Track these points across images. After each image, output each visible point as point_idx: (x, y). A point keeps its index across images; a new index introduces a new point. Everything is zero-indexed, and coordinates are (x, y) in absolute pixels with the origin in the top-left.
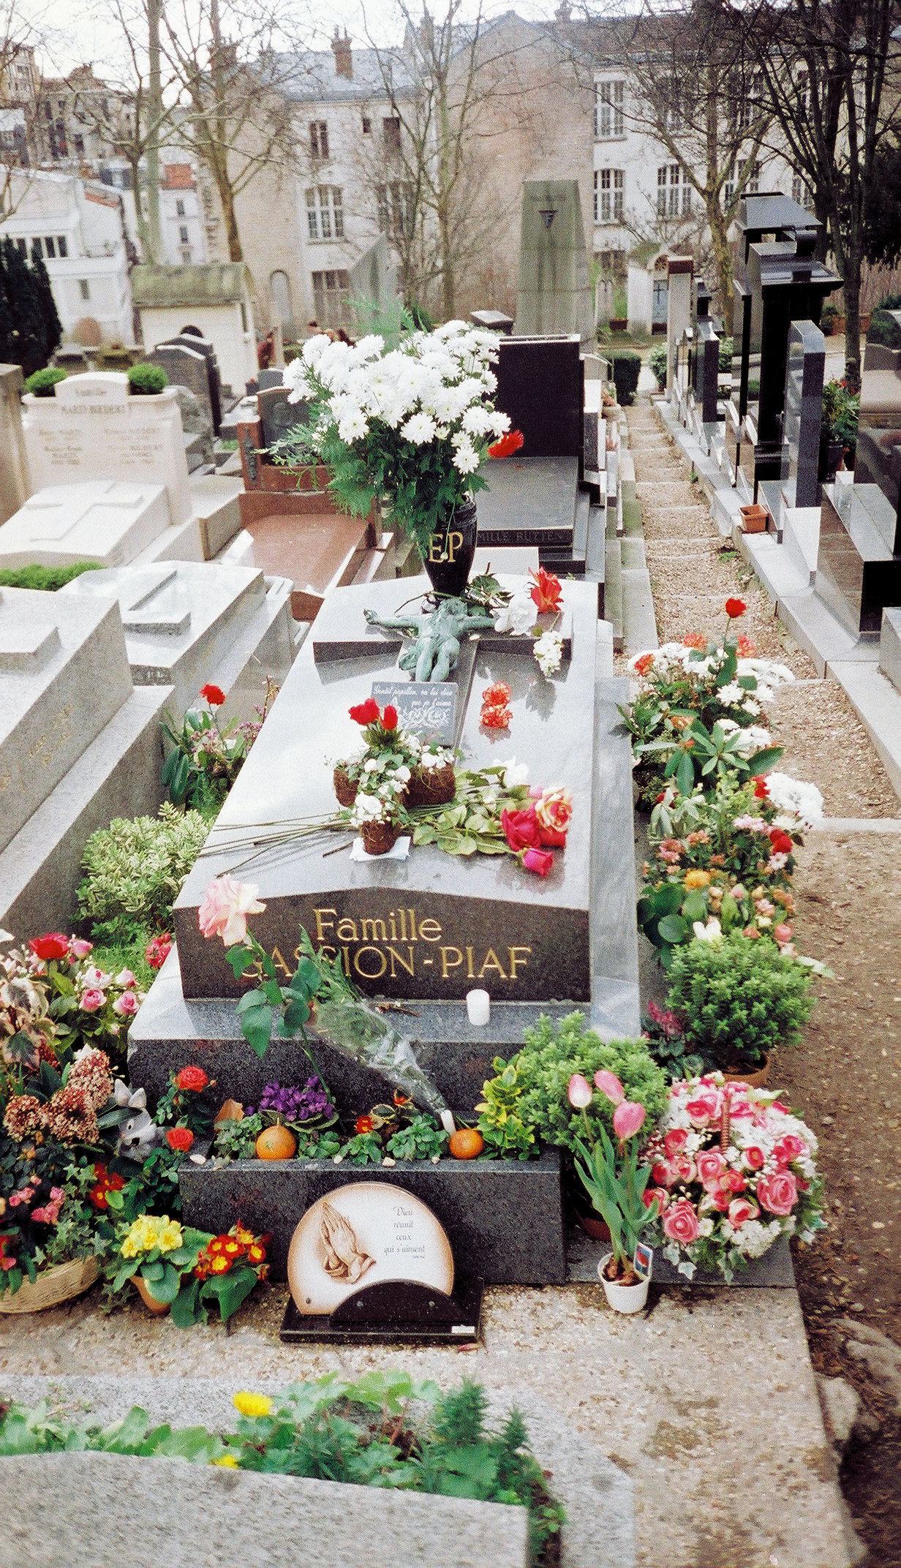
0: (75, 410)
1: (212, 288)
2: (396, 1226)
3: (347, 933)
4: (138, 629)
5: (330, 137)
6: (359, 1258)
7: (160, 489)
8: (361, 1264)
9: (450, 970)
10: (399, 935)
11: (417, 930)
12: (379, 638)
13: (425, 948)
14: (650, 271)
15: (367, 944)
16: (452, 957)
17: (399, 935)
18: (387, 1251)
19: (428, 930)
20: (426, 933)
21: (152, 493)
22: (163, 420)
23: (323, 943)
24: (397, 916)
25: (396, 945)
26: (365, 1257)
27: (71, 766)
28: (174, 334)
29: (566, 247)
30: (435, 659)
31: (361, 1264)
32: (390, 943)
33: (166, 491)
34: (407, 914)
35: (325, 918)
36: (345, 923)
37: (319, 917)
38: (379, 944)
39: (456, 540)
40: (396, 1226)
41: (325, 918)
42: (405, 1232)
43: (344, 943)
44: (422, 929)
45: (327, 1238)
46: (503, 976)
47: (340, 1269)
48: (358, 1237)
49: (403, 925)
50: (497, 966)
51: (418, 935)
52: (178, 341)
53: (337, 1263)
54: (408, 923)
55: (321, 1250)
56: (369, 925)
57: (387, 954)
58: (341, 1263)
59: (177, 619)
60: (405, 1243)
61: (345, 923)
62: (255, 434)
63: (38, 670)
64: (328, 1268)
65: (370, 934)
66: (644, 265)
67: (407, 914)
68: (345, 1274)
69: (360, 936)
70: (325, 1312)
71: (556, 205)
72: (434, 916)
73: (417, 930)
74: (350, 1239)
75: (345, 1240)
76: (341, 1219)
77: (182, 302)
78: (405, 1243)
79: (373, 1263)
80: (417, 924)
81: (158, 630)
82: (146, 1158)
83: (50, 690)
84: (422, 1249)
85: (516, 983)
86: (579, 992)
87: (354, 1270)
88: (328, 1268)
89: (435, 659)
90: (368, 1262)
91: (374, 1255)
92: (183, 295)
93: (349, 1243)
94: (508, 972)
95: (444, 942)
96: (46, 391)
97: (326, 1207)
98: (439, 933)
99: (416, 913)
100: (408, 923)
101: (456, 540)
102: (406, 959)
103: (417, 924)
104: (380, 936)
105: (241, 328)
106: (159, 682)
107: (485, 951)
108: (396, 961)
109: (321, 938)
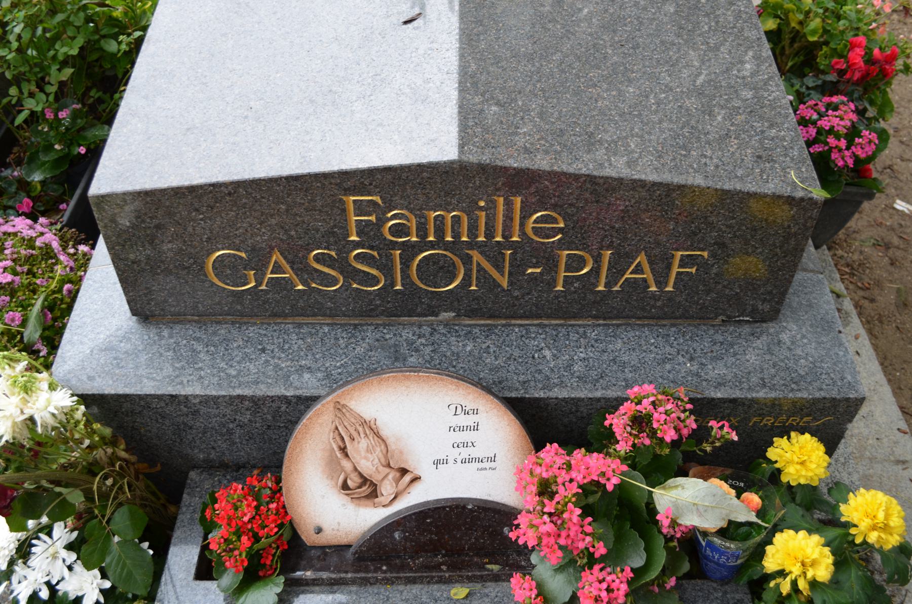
6: (393, 475)
8: (397, 481)
11: (522, 225)
13: (528, 252)
15: (432, 246)
16: (576, 263)
17: (490, 234)
18: (437, 463)
23: (357, 245)
24: (491, 207)
25: (480, 247)
26: (404, 471)
31: (397, 481)
32: (480, 247)
34: (509, 204)
35: (360, 208)
36: (395, 217)
37: (351, 207)
41: (360, 208)
43: (394, 245)
44: (530, 223)
45: (343, 450)
46: (653, 288)
47: (365, 489)
48: (392, 447)
49: (500, 218)
50: (648, 275)
51: (523, 233)
53: (358, 480)
54: (509, 218)
55: (332, 466)
56: (440, 220)
58: (365, 481)
60: (465, 453)
61: (395, 217)
64: (345, 486)
65: (440, 232)
67: (509, 204)
68: (373, 494)
70: (344, 541)
72: (554, 207)
73: (522, 225)
75: (368, 450)
76: (364, 423)
78: (465, 453)
79: (416, 479)
80: (524, 218)
84: (493, 459)
85: (670, 297)
87: (387, 489)
90: (407, 478)
91: (421, 465)
95: (561, 245)
97: (340, 408)
98: (561, 230)
100: (509, 218)
103: (524, 218)
108: (480, 269)
109: (354, 238)
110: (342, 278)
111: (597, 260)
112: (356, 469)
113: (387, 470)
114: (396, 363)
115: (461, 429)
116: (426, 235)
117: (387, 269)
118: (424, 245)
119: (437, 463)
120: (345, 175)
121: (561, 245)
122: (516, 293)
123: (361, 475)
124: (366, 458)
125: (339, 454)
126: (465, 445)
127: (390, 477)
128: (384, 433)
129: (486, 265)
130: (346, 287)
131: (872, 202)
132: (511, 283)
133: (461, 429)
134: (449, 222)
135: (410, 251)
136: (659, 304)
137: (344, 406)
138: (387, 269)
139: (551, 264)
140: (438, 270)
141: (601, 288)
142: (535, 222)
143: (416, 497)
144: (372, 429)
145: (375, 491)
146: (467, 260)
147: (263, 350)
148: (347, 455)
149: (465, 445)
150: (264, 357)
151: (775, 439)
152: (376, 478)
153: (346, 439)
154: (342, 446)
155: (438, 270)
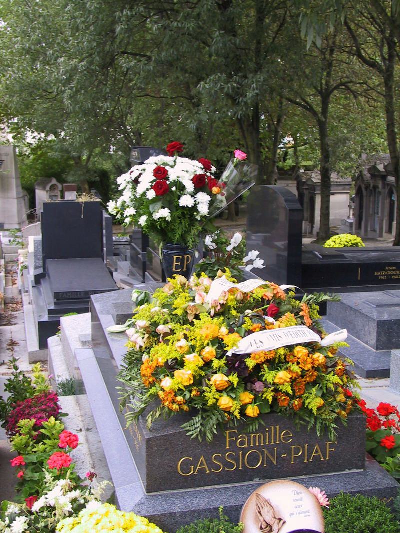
2: (295, 500)
11: (280, 436)
14: (47, 191)
15: (252, 448)
17: (270, 442)
18: (291, 514)
23: (229, 450)
26: (280, 519)
34: (275, 429)
40: (295, 500)
45: (260, 512)
50: (320, 453)
54: (276, 434)
60: (300, 509)
66: (44, 189)
67: (275, 429)
69: (249, 444)
73: (280, 436)
74: (272, 511)
75: (268, 512)
78: (300, 509)
82: (218, 419)
86: (360, 463)
88: (261, 528)
90: (282, 522)
91: (286, 517)
93: (271, 513)
94: (325, 456)
97: (258, 495)
98: (291, 437)
102: (273, 455)
103: (280, 433)
108: (267, 457)
110: (222, 466)
111: (304, 449)
112: (265, 520)
113: (275, 519)
115: (297, 500)
116: (256, 444)
118: (250, 448)
119: (291, 514)
122: (279, 466)
123: (267, 522)
124: (268, 515)
125: (258, 514)
126: (299, 506)
127: (276, 522)
128: (273, 504)
129: (270, 456)
130: (224, 469)
132: (277, 462)
133: (297, 500)
134: (257, 437)
135: (245, 451)
136: (325, 466)
137: (259, 494)
138: (237, 460)
139: (289, 451)
140: (254, 459)
141: (306, 461)
142: (284, 435)
145: (271, 529)
146: (263, 453)
147: (197, 497)
148: (261, 515)
149: (299, 506)
150: (198, 499)
152: (271, 523)
153: (261, 507)
155: (254, 459)
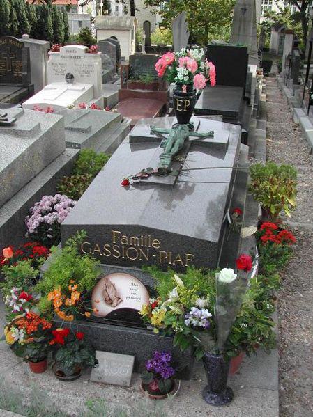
0: (65, 57)
1: (122, 24)
3: (124, 241)
4: (72, 130)
5: (77, 134)
6: (117, 299)
7: (91, 86)
9: (162, 260)
10: (144, 245)
12: (155, 136)
13: (154, 251)
15: (131, 246)
19: (156, 244)
20: (155, 245)
21: (88, 87)
22: (95, 62)
26: (119, 298)
27: (30, 181)
28: (108, 37)
29: (249, 21)
30: (173, 145)
33: (93, 86)
38: (136, 247)
39: (187, 103)
41: (117, 234)
42: (135, 292)
43: (123, 245)
45: (106, 290)
47: (109, 302)
52: (108, 40)
55: (103, 295)
57: (139, 251)
59: (86, 127)
62: (127, 69)
63: (32, 137)
68: (112, 303)
71: (247, 7)
77: (111, 29)
79: (122, 301)
81: (79, 130)
83: (33, 145)
87: (115, 303)
89: (173, 145)
91: (124, 298)
92: (112, 26)
95: (160, 249)
96: (56, 50)
97: (107, 280)
99: (151, 237)
101: (187, 103)
103: (152, 241)
104: (137, 244)
105: (131, 38)
106: (75, 148)
107: (177, 254)
114: (117, 271)
117: (121, 252)
120: (114, 226)
121: (160, 249)
131: (191, 196)
143: (121, 306)
144: (113, 286)
151: (100, 355)
154: (88, 289)
